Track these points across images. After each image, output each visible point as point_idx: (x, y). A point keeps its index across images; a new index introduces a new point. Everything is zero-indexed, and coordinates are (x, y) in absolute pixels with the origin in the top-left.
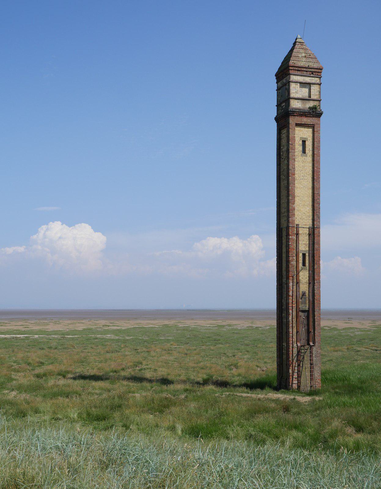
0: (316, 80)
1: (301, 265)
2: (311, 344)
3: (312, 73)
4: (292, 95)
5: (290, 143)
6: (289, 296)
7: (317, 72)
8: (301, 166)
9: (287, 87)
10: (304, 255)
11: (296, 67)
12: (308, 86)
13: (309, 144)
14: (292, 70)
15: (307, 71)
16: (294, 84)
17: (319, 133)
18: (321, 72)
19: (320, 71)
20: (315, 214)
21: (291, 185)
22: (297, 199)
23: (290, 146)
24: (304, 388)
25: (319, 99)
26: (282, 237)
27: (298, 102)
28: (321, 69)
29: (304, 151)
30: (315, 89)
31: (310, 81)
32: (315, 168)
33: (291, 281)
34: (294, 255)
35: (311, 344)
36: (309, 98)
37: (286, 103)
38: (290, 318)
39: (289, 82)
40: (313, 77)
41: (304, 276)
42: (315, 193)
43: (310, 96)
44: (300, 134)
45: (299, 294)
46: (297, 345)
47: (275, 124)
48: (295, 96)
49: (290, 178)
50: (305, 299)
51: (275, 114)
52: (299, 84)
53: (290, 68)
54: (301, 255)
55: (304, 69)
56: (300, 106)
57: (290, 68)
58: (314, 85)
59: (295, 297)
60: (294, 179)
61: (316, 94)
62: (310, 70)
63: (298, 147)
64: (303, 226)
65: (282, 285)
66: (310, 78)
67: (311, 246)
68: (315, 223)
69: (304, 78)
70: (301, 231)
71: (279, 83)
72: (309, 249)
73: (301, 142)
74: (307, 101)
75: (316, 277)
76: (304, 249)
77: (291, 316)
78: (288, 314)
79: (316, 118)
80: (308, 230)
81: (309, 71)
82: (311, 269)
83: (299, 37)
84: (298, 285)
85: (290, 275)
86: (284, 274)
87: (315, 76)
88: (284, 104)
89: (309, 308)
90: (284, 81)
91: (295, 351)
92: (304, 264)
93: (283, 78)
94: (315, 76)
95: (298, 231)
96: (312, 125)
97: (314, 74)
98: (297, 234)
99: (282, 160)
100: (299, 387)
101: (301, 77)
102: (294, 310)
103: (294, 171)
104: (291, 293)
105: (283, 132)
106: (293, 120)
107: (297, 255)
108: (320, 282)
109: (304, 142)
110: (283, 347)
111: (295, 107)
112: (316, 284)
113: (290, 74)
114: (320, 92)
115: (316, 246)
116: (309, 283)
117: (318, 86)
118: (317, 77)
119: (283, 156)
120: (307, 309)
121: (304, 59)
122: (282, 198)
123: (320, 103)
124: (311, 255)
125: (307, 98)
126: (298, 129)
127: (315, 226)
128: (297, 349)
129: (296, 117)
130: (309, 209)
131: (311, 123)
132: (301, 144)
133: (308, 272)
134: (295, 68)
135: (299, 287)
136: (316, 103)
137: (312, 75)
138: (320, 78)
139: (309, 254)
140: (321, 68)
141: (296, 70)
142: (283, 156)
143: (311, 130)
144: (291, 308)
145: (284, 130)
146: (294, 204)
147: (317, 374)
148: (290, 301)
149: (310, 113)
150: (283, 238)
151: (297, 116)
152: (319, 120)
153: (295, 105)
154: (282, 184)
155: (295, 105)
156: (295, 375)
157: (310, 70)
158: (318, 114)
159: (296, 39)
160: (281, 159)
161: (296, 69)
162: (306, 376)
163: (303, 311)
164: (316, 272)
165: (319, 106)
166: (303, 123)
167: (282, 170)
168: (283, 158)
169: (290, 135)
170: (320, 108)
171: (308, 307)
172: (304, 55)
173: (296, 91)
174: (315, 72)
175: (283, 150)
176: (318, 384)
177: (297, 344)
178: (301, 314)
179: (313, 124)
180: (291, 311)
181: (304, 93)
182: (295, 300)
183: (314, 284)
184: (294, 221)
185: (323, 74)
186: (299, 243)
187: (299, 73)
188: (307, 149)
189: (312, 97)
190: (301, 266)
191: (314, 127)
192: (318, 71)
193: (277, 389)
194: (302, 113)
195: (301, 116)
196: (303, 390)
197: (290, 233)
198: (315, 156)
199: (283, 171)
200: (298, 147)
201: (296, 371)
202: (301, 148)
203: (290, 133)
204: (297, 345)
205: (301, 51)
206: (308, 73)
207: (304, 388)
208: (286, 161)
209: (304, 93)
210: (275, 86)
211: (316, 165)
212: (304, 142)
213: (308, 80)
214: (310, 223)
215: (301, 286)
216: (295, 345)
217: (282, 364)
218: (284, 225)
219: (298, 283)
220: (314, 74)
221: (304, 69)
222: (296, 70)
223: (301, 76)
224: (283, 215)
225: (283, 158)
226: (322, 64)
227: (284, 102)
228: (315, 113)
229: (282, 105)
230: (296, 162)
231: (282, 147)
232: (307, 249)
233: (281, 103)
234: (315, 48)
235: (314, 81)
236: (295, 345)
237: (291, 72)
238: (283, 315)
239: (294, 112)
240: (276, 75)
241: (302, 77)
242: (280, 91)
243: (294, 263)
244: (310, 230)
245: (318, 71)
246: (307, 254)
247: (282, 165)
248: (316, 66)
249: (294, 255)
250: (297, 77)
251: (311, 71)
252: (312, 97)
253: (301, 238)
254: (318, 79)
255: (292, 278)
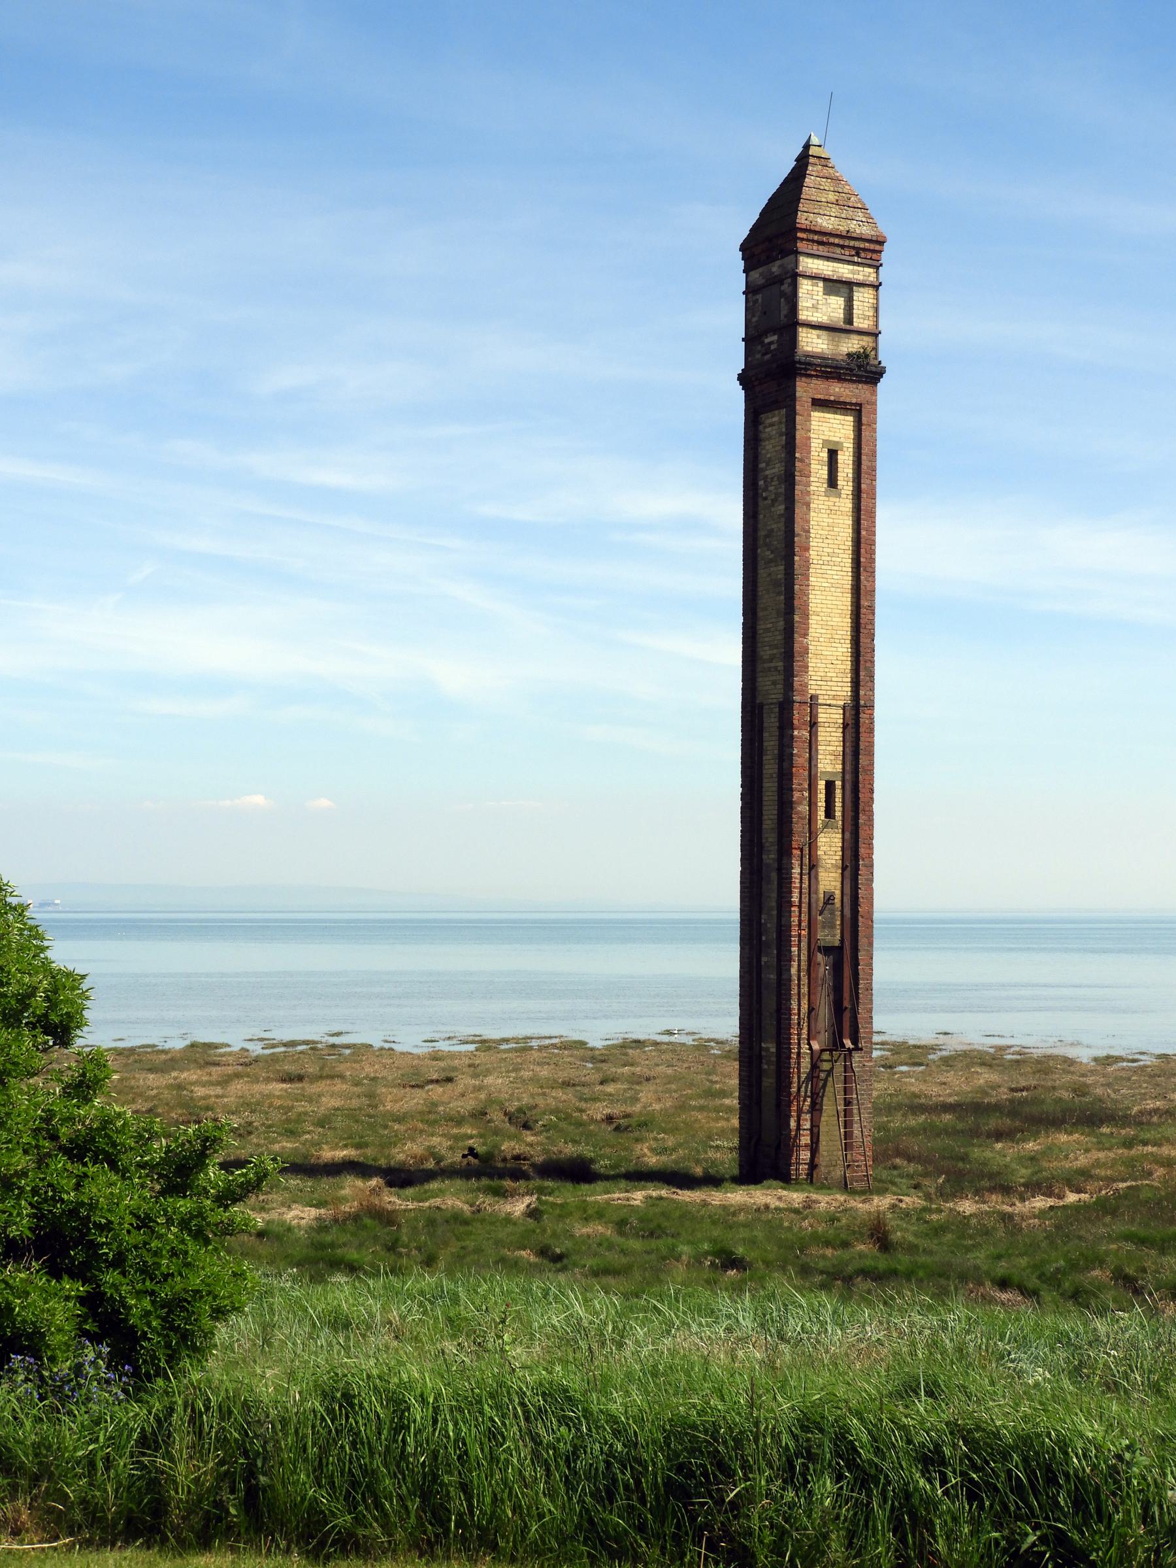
0: (864, 274)
1: (821, 814)
2: (848, 1043)
3: (858, 251)
4: (803, 315)
5: (797, 455)
6: (791, 904)
7: (867, 250)
8: (825, 523)
9: (785, 287)
10: (830, 786)
11: (816, 232)
12: (845, 290)
13: (846, 460)
14: (802, 239)
15: (843, 247)
16: (810, 282)
17: (875, 430)
18: (880, 252)
19: (878, 247)
20: (862, 667)
21: (798, 579)
22: (813, 620)
23: (797, 464)
24: (829, 1172)
25: (872, 329)
26: (761, 731)
27: (818, 337)
28: (881, 243)
29: (832, 482)
30: (863, 299)
31: (851, 276)
32: (863, 533)
33: (796, 863)
34: (796, 783)
35: (848, 1043)
36: (848, 327)
37: (780, 336)
38: (794, 971)
39: (794, 276)
40: (858, 264)
41: (830, 845)
42: (862, 602)
43: (849, 318)
44: (826, 430)
45: (818, 900)
46: (811, 1048)
47: (739, 394)
48: (810, 319)
49: (796, 558)
50: (832, 913)
51: (741, 365)
52: (821, 284)
53: (799, 235)
54: (822, 785)
55: (837, 241)
56: (825, 347)
57: (799, 235)
58: (861, 289)
59: (805, 909)
60: (807, 564)
61: (867, 313)
62: (852, 243)
63: (818, 471)
64: (828, 702)
65: (760, 871)
66: (851, 267)
67: (849, 758)
68: (862, 693)
69: (836, 265)
70: (823, 716)
71: (755, 274)
72: (843, 768)
73: (825, 455)
74: (843, 335)
75: (862, 851)
76: (829, 769)
77: (795, 964)
78: (783, 958)
79: (865, 387)
80: (841, 712)
81: (849, 247)
82: (849, 827)
83: (815, 140)
84: (813, 872)
85: (794, 845)
86: (770, 840)
87: (864, 261)
88: (775, 338)
89: (842, 940)
90: (775, 268)
91: (806, 1063)
92: (829, 813)
93: (770, 260)
94: (864, 261)
95: (816, 716)
96: (856, 404)
97: (863, 255)
98: (813, 725)
99: (761, 503)
100: (813, 1166)
101: (826, 263)
102: (804, 945)
103: (808, 538)
104: (795, 898)
105: (769, 421)
106: (805, 389)
107: (812, 788)
108: (872, 866)
109: (833, 454)
110: (764, 1053)
111: (810, 349)
112: (862, 871)
113: (797, 253)
114: (876, 310)
115: (863, 761)
116: (844, 868)
117: (871, 291)
118: (870, 266)
119: (766, 489)
120: (837, 944)
121: (834, 210)
122: (760, 614)
123: (876, 342)
124: (848, 786)
125: (841, 324)
126: (816, 415)
127: (862, 702)
128: (812, 1058)
129: (814, 381)
130: (844, 649)
131: (854, 401)
132: (826, 459)
133: (840, 836)
134: (811, 236)
135: (817, 878)
136: (866, 341)
137: (856, 259)
138: (877, 268)
139: (843, 781)
140: (880, 239)
141: (813, 241)
142: (766, 489)
143: (851, 418)
144: (794, 940)
145: (770, 414)
146: (805, 635)
147: (863, 1129)
148: (795, 920)
149: (851, 370)
150: (766, 735)
151: (817, 376)
152: (874, 393)
153: (811, 343)
154: (762, 573)
155: (811, 343)
156: (805, 1139)
157: (852, 243)
158: (872, 372)
159: (807, 146)
160: (760, 500)
161: (816, 238)
162: (820, 1132)
163: (827, 950)
164: (862, 833)
165: (875, 349)
166: (832, 398)
167: (762, 533)
168: (766, 499)
169: (797, 433)
170: (876, 357)
171: (838, 937)
172: (832, 197)
173: (815, 304)
174: (864, 250)
175: (767, 472)
176: (862, 1156)
177: (809, 1044)
178: (820, 957)
179: (859, 401)
180: (795, 949)
181: (831, 309)
182: (804, 917)
183: (858, 869)
184: (806, 685)
185: (885, 257)
186: (817, 750)
187: (822, 250)
188: (841, 476)
189: (858, 323)
190: (823, 817)
191: (860, 411)
192: (872, 246)
193: (750, 1175)
194: (831, 370)
195: (827, 378)
196: (826, 1179)
197: (795, 722)
198: (864, 496)
199: (767, 536)
200: (818, 471)
201: (808, 1126)
202: (824, 472)
203: (798, 427)
204: (811, 1048)
205: (826, 184)
206: (847, 253)
207: (829, 1172)
208: (783, 507)
209: (831, 309)
210: (739, 282)
211: (864, 523)
212: (833, 454)
213: (845, 271)
214: (845, 690)
215: (822, 875)
216: (805, 1048)
217: (759, 1103)
218: (771, 692)
219: (813, 866)
220: (863, 255)
221: (837, 241)
222: (813, 241)
223: (828, 259)
224: (766, 665)
225: (766, 499)
226: (885, 228)
227: (774, 331)
228: (865, 370)
229: (767, 341)
230: (812, 514)
231: (762, 465)
232: (839, 767)
233: (766, 333)
234: (868, 176)
235: (860, 278)
236: (805, 1048)
237: (801, 246)
238: (764, 959)
239: (810, 364)
240: (744, 248)
241: (830, 264)
242: (759, 297)
243: (803, 808)
244: (847, 714)
245: (872, 246)
246: (838, 783)
247: (761, 517)
248: (865, 231)
249: (796, 783)
250: (816, 261)
251: (854, 248)
252: (858, 323)
253: (822, 734)
254: (871, 270)
255: (798, 852)
